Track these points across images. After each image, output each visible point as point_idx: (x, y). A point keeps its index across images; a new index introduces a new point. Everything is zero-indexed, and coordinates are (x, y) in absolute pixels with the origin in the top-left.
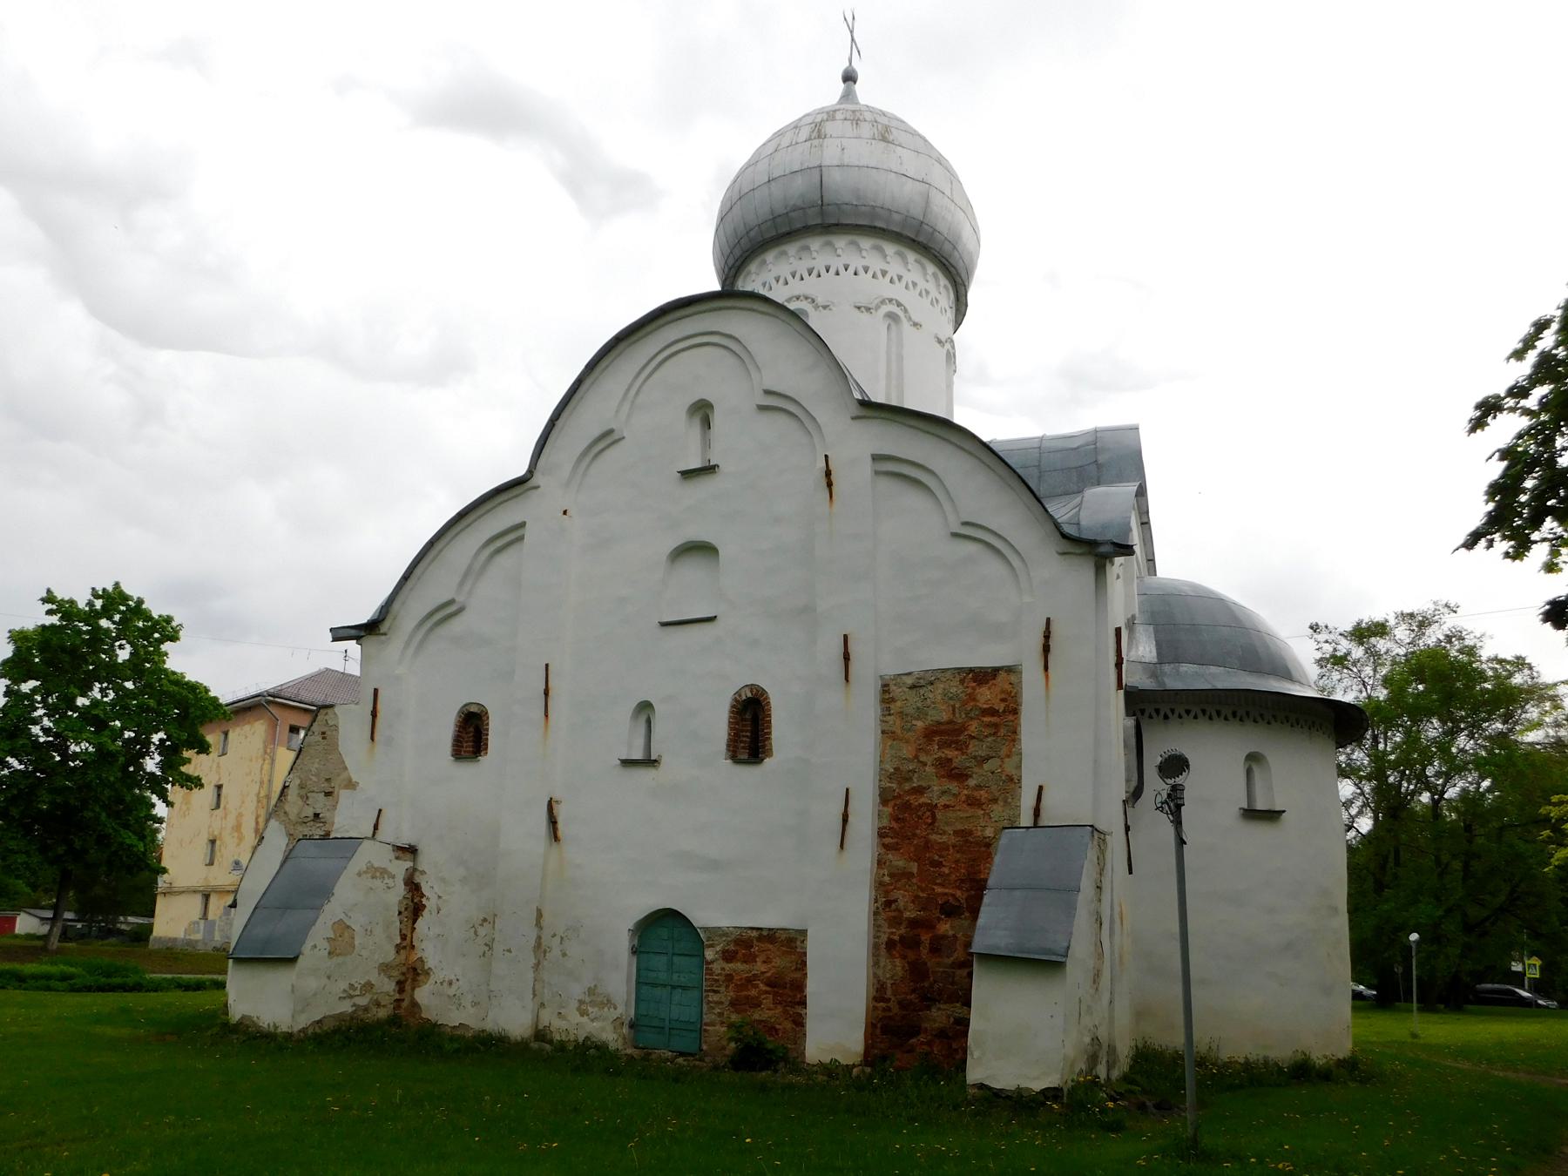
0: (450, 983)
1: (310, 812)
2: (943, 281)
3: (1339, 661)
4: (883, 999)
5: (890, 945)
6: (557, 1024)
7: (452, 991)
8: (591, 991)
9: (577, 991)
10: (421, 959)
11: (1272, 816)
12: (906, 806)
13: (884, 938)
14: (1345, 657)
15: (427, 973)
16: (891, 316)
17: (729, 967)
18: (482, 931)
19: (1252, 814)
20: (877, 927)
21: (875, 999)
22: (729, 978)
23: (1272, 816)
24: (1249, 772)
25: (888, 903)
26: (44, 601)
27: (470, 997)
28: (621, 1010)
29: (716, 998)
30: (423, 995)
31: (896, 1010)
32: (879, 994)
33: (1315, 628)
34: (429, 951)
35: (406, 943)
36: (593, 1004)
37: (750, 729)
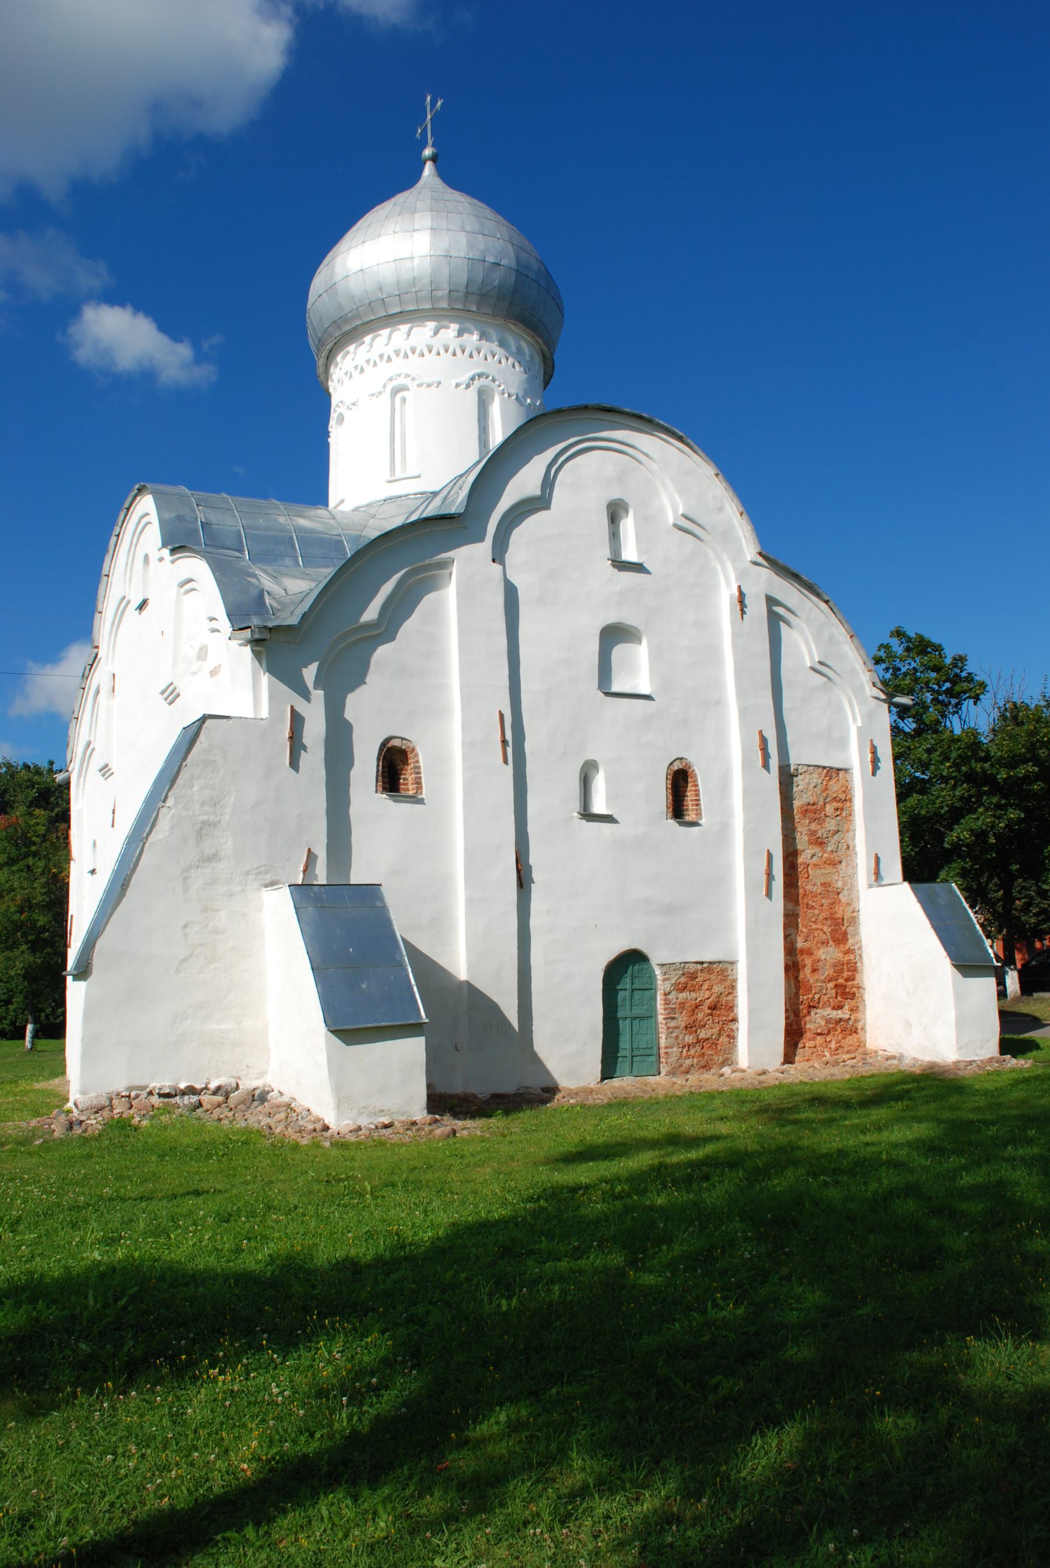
17: (682, 996)
22: (682, 1005)
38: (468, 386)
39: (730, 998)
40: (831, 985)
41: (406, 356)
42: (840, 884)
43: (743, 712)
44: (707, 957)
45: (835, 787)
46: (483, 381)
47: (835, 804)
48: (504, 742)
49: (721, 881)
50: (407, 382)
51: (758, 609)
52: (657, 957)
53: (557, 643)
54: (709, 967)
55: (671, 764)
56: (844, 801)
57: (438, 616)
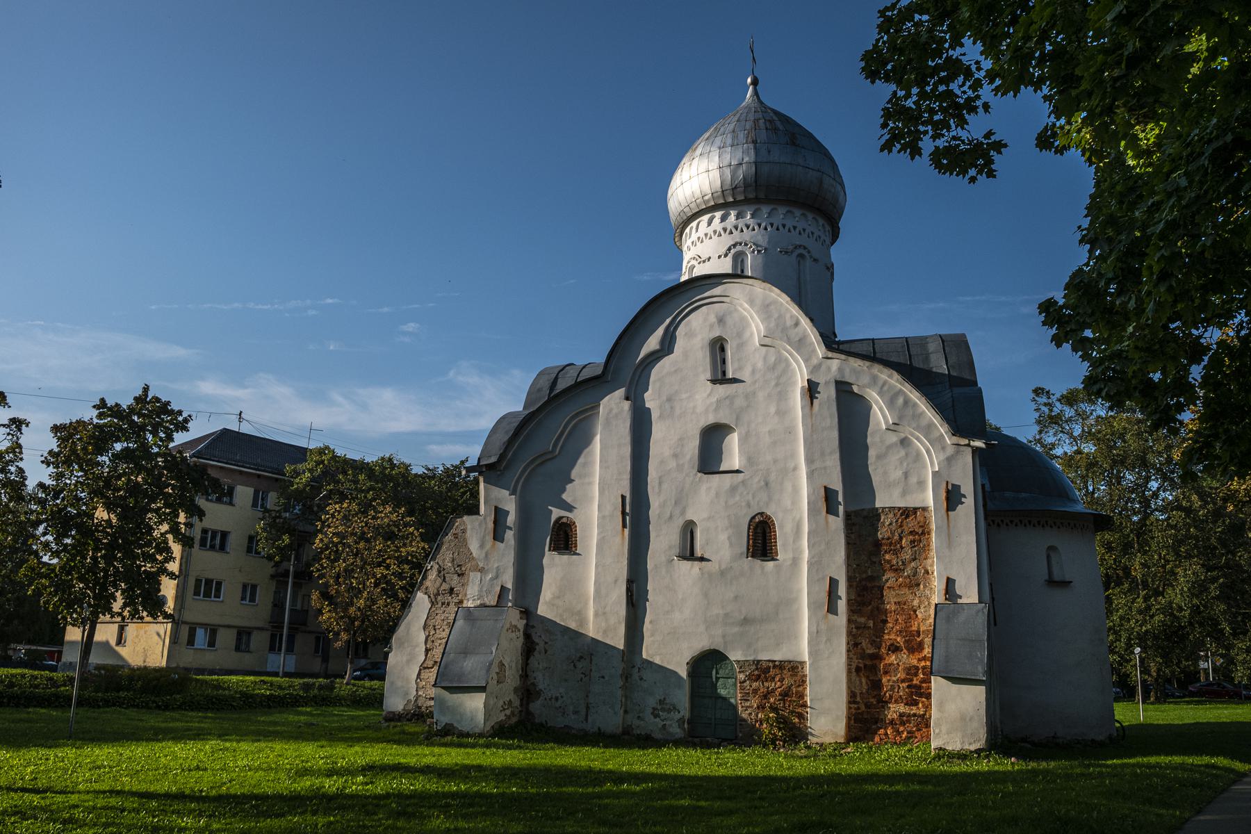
0: (557, 699)
1: (445, 586)
2: (828, 228)
3: (1055, 420)
4: (855, 702)
5: (858, 670)
6: (636, 722)
7: (558, 704)
8: (661, 702)
9: (652, 702)
10: (533, 684)
11: (1065, 584)
12: (865, 588)
13: (854, 666)
14: (1059, 416)
15: (539, 693)
16: (801, 256)
17: (755, 685)
18: (580, 665)
19: (1052, 582)
20: (849, 658)
21: (850, 702)
22: (755, 691)
23: (1065, 584)
24: (1048, 557)
25: (856, 645)
26: (186, 421)
27: (571, 708)
28: (682, 713)
29: (748, 704)
30: (536, 707)
31: (863, 708)
32: (852, 698)
33: (1038, 391)
34: (541, 680)
35: (525, 674)
36: (663, 710)
37: (761, 539)
38: (726, 255)
39: (800, 689)
40: (905, 685)
41: (731, 233)
42: (916, 603)
43: (810, 475)
44: (778, 657)
45: (911, 524)
46: (739, 248)
47: (911, 537)
48: (624, 513)
49: (787, 602)
50: (739, 248)
51: (828, 393)
52: (735, 655)
53: (672, 441)
54: (781, 666)
55: (753, 518)
56: (924, 531)
57: (875, 413)
